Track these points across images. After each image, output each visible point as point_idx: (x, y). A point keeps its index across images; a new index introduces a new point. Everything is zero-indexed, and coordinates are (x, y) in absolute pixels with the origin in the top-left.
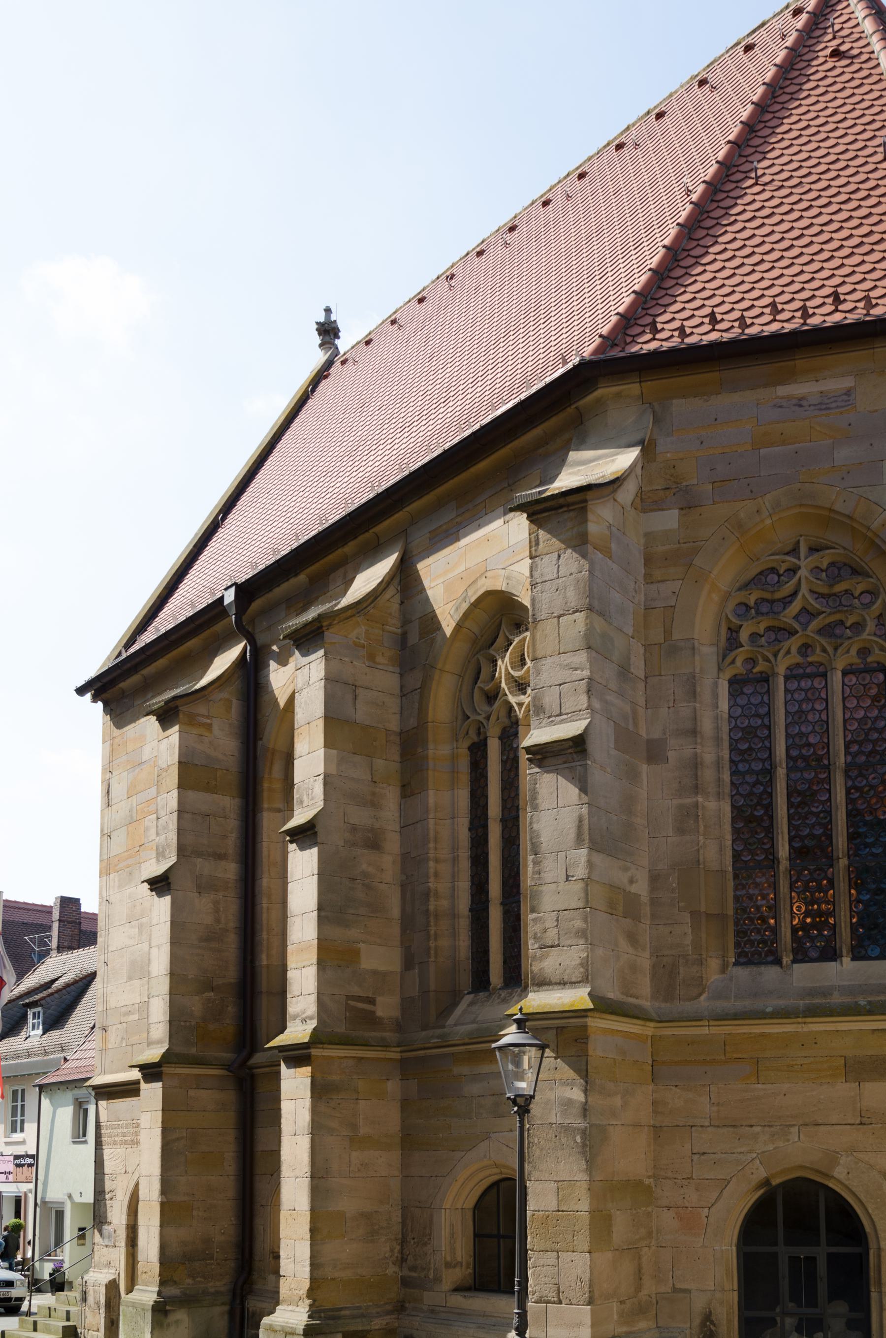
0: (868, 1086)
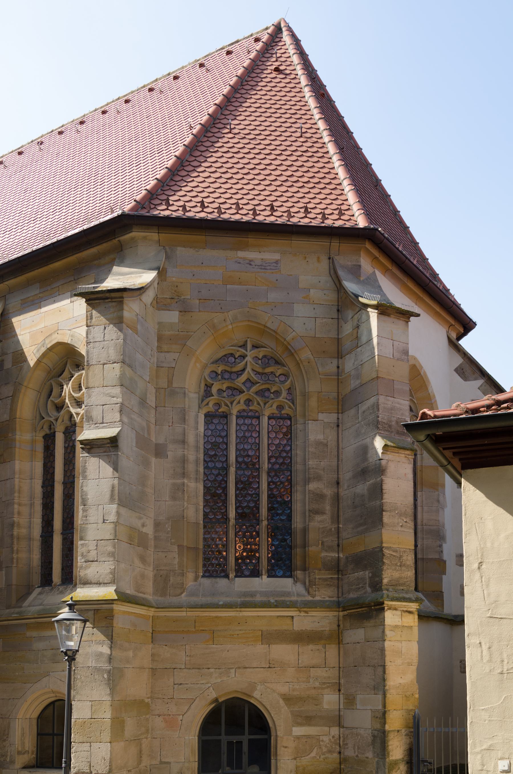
0: (274, 647)
